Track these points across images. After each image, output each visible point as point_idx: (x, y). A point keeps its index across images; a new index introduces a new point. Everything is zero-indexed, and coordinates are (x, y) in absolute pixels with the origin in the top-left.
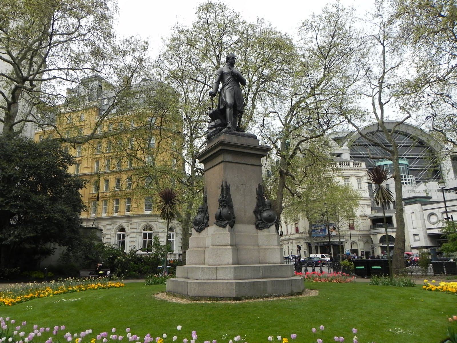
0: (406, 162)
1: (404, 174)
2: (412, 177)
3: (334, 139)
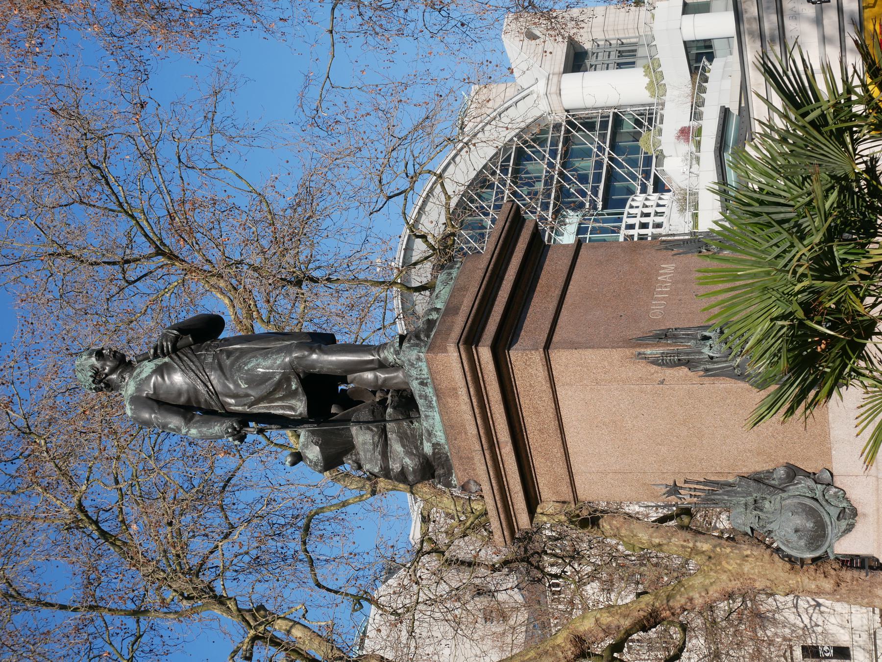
0: (573, 219)
1: (616, 230)
2: (634, 204)
3: (539, 38)
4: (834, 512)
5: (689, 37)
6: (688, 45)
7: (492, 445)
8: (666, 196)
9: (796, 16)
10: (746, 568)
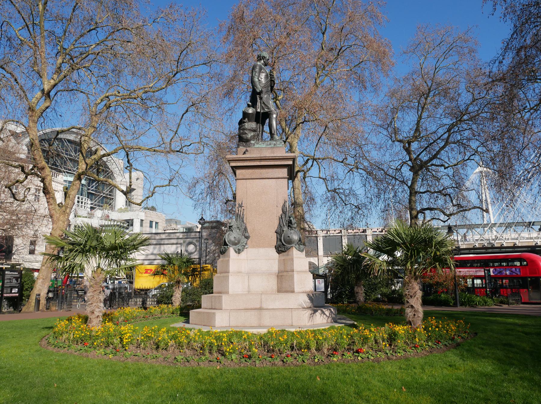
4: (239, 248)
5: (134, 221)
6: (132, 220)
7: (261, 160)
8: (89, 210)
9: (154, 248)
10: (61, 222)
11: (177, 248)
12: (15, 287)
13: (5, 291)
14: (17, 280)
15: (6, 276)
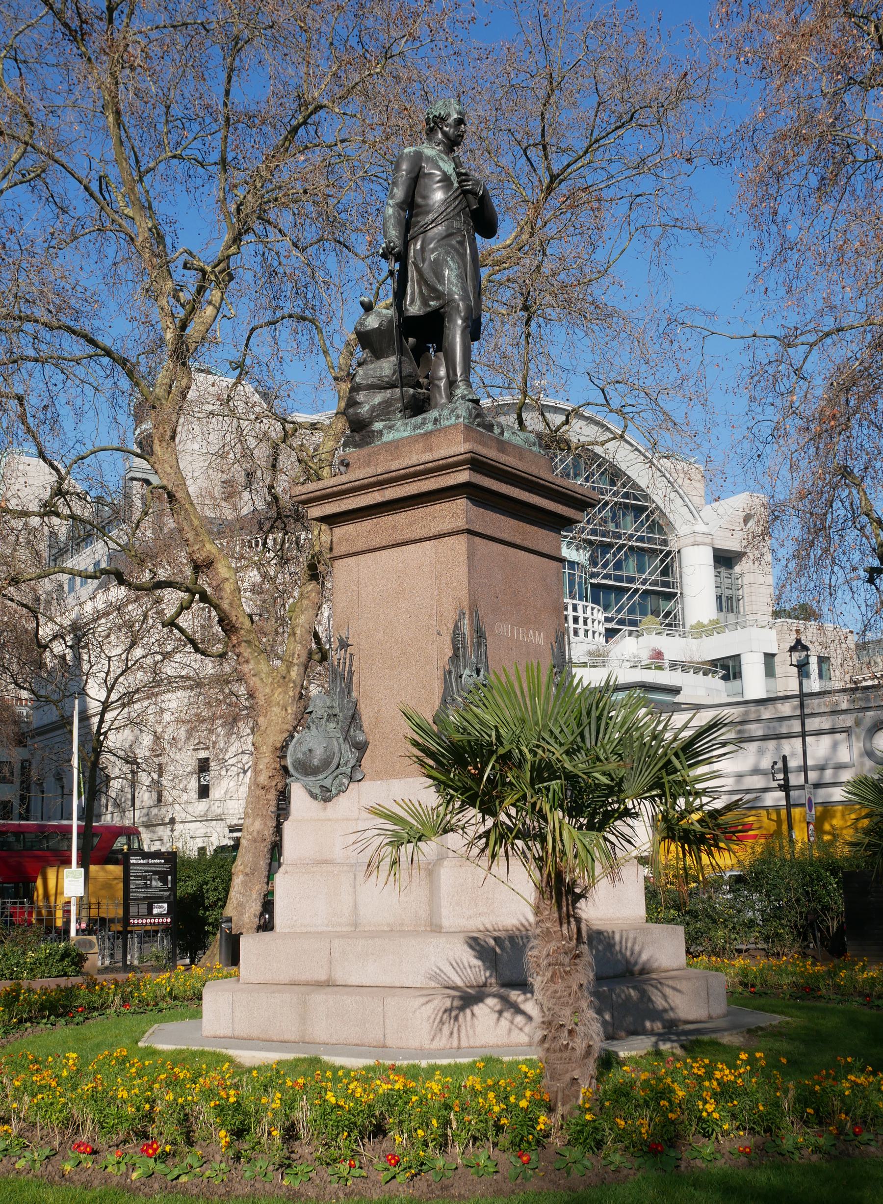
4: (327, 783)
5: (744, 660)
7: (381, 484)
8: (602, 640)
9: (761, 752)
10: (276, 709)
11: (835, 746)
12: (160, 900)
13: (133, 910)
14: (164, 880)
15: (132, 869)
